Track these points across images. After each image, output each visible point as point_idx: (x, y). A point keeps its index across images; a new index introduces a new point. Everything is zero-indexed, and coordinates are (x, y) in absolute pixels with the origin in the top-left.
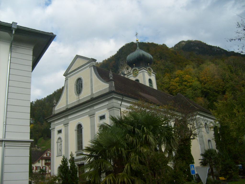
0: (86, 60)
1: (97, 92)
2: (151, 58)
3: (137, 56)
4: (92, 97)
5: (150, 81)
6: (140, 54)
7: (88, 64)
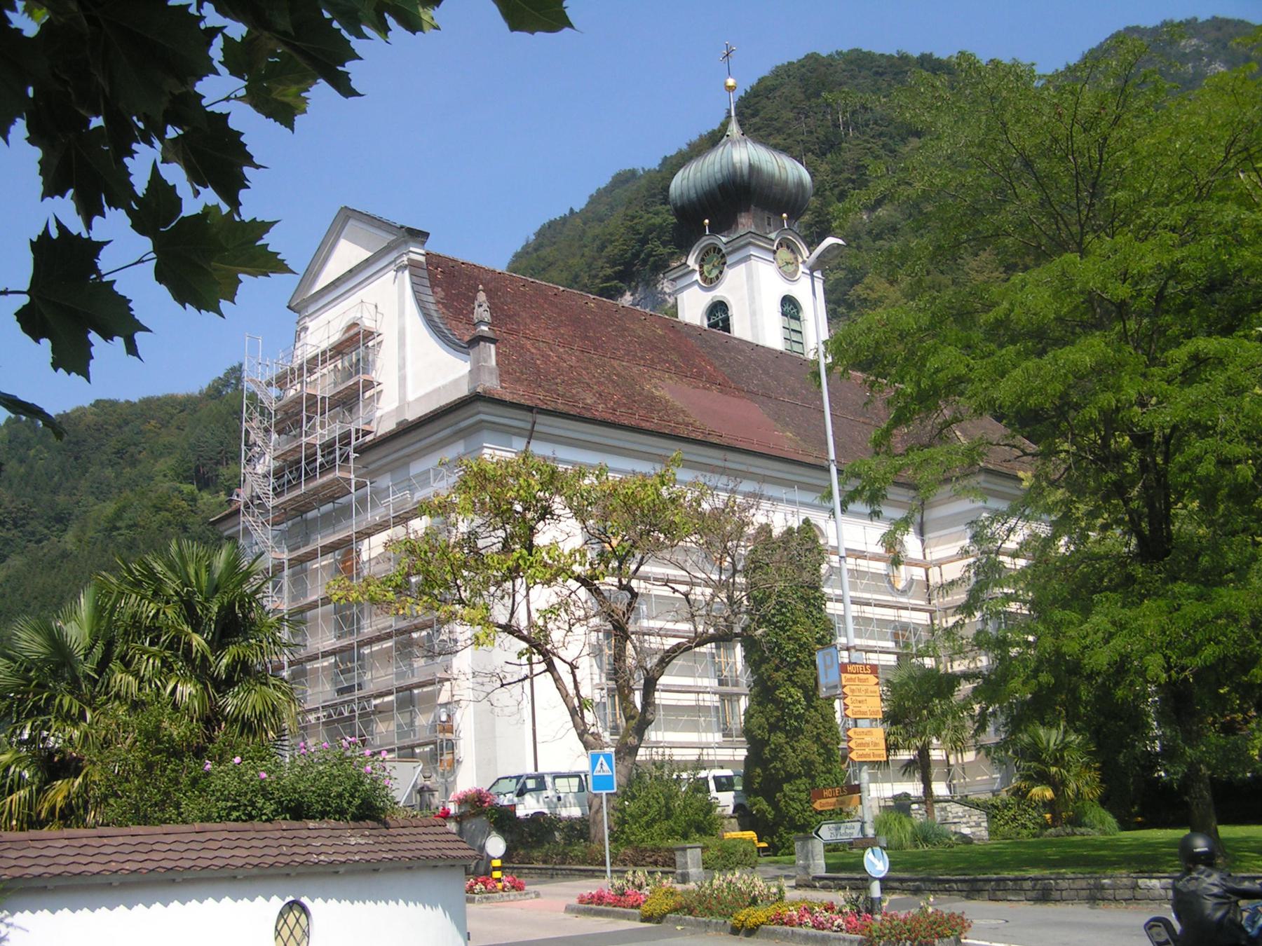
0: (384, 234)
1: (423, 393)
2: (800, 184)
3: (719, 176)
4: (402, 419)
5: (790, 307)
6: (738, 165)
7: (388, 253)
